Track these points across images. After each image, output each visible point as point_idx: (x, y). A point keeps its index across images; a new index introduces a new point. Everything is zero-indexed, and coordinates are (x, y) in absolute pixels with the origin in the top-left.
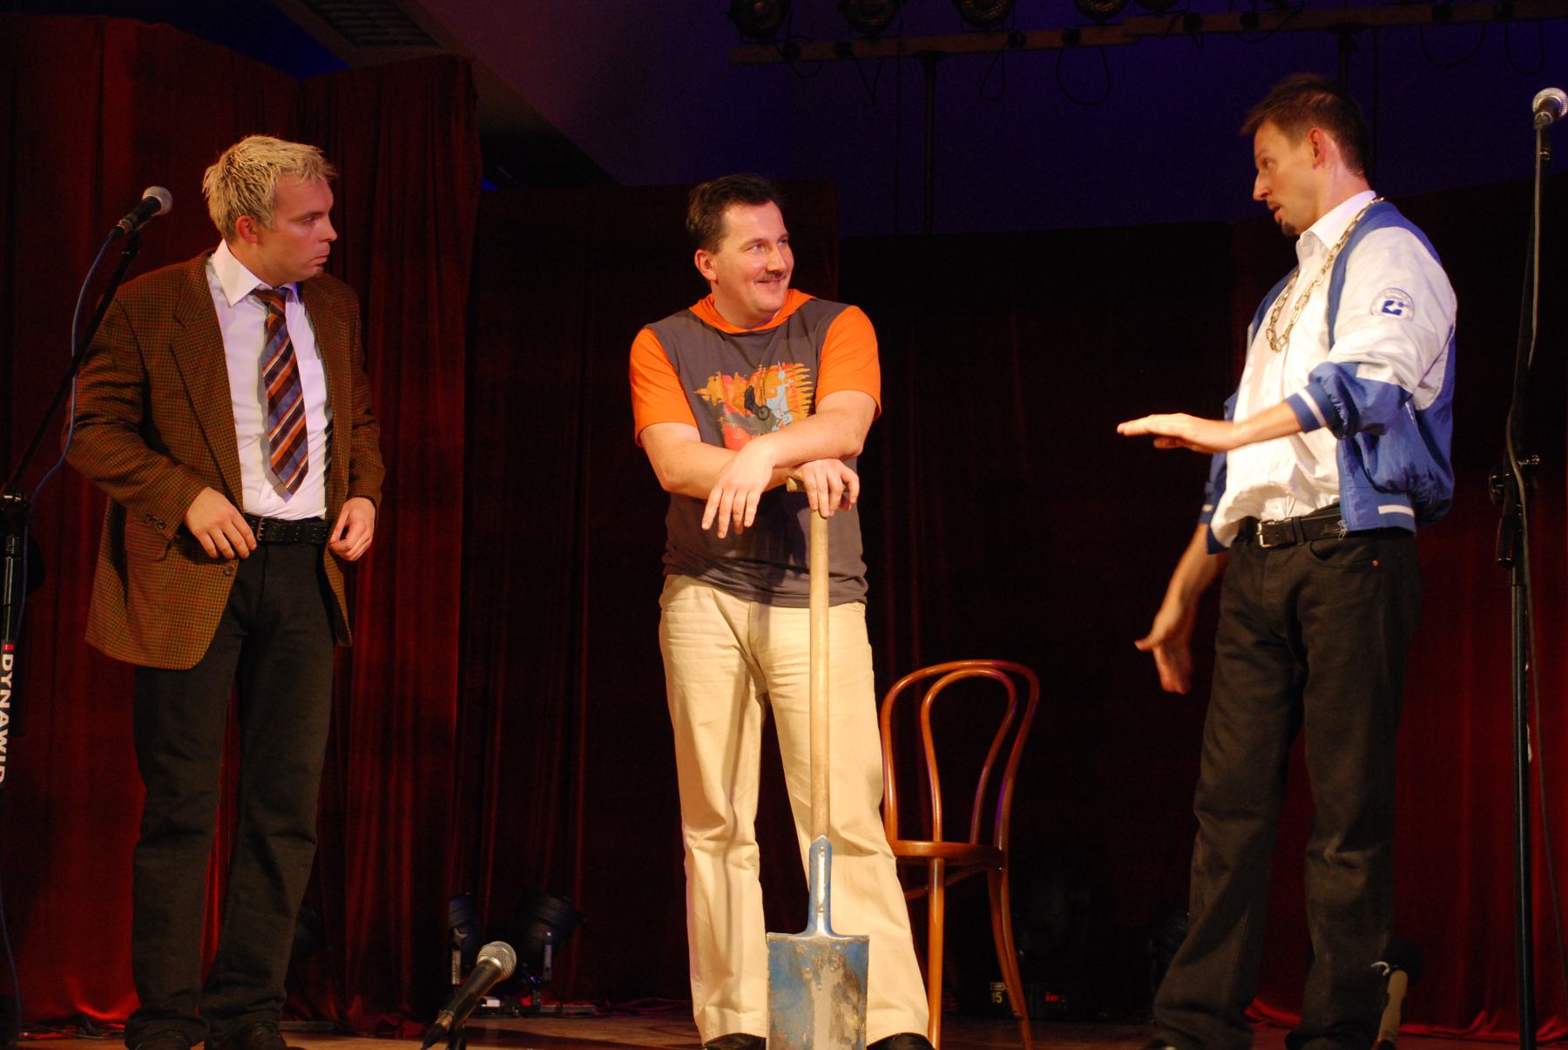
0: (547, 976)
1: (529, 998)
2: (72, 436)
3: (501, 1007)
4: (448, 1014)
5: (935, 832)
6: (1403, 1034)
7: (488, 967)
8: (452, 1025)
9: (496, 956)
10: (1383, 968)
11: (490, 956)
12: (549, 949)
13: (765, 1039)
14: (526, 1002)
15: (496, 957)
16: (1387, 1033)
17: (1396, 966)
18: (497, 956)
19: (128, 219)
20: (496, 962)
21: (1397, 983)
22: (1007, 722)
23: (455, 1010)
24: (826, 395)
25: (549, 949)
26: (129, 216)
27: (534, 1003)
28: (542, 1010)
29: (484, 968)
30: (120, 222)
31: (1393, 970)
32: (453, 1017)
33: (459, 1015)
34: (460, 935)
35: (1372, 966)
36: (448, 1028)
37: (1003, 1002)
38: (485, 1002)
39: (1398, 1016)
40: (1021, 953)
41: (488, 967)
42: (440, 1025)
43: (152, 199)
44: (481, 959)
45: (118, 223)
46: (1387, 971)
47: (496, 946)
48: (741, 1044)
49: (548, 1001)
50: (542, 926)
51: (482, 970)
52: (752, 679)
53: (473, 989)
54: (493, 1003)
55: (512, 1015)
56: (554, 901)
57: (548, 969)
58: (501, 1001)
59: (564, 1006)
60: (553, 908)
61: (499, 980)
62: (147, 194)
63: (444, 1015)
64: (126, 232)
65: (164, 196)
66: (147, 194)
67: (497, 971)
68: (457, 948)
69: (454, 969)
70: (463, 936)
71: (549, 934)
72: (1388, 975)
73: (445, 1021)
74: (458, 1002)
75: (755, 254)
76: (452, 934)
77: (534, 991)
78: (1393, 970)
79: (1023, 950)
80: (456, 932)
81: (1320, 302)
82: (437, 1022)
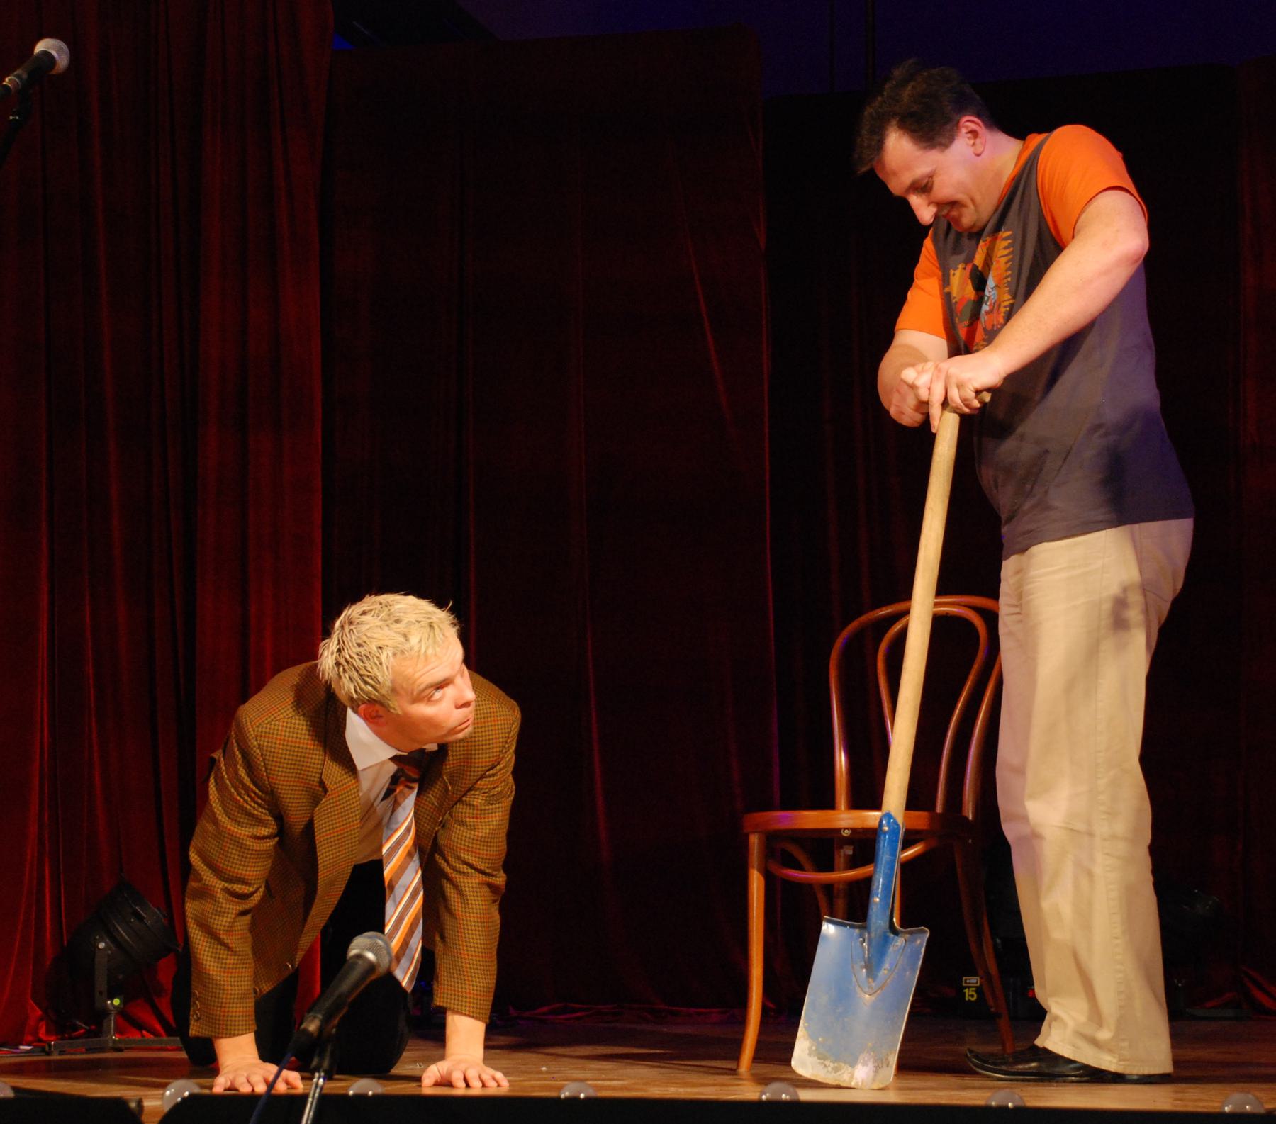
4: (315, 1017)
5: (761, 985)
7: (360, 962)
8: (321, 1029)
9: (370, 949)
11: (363, 949)
13: (877, 806)
15: (369, 950)
19: (18, 76)
20: (370, 956)
22: (839, 875)
23: (323, 1012)
26: (16, 73)
29: (356, 964)
30: (7, 79)
32: (321, 1021)
36: (315, 1035)
37: (977, 999)
40: (998, 941)
41: (360, 962)
42: (305, 1030)
43: (46, 54)
44: (353, 952)
45: (4, 81)
47: (369, 937)
51: (353, 966)
61: (373, 977)
62: (40, 47)
63: (310, 1019)
64: (13, 90)
65: (59, 50)
66: (40, 47)
75: (968, 145)
79: (1000, 938)
81: (1012, 612)
82: (303, 1027)
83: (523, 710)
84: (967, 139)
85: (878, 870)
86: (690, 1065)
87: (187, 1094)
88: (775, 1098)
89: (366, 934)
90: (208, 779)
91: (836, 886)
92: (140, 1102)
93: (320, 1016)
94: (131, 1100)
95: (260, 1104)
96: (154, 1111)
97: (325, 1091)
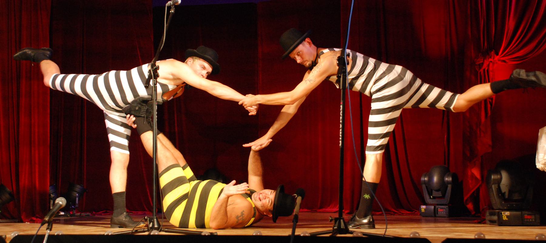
0: (77, 206)
1: (72, 212)
2: (251, 226)
3: (64, 214)
4: (47, 217)
6: (300, 212)
8: (49, 220)
10: (295, 196)
12: (77, 199)
14: (71, 213)
15: (60, 201)
16: (296, 212)
17: (298, 195)
18: (61, 201)
21: (299, 200)
24: (141, 135)
25: (77, 199)
27: (74, 213)
28: (76, 215)
31: (298, 196)
33: (50, 217)
34: (52, 196)
35: (293, 195)
38: (60, 213)
39: (299, 208)
46: (296, 196)
48: (349, 73)
49: (77, 212)
50: (75, 193)
52: (186, 201)
53: (55, 210)
54: (62, 213)
55: (67, 216)
56: (78, 186)
57: (77, 204)
58: (64, 213)
59: (82, 214)
60: (78, 188)
61: (61, 208)
67: (61, 205)
68: (52, 199)
69: (51, 205)
70: (53, 196)
71: (77, 195)
72: (297, 198)
73: (47, 219)
74: (50, 213)
76: (50, 195)
77: (73, 210)
78: (298, 196)
80: (51, 195)
83: (46, 86)
84: (348, 66)
85: (20, 146)
86: (124, 231)
87: (17, 235)
88: (154, 234)
89: (60, 198)
90: (200, 180)
91: (443, 211)
92: (6, 236)
93: (49, 217)
94: (3, 235)
95: (35, 237)
96: (9, 238)
97: (50, 234)
